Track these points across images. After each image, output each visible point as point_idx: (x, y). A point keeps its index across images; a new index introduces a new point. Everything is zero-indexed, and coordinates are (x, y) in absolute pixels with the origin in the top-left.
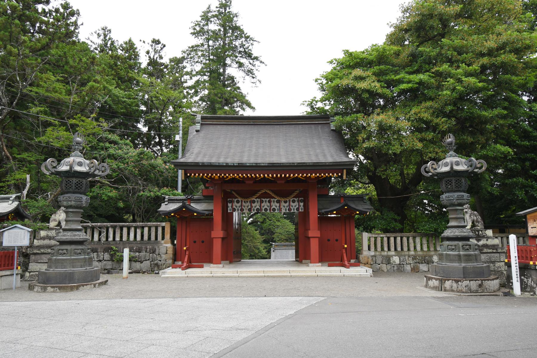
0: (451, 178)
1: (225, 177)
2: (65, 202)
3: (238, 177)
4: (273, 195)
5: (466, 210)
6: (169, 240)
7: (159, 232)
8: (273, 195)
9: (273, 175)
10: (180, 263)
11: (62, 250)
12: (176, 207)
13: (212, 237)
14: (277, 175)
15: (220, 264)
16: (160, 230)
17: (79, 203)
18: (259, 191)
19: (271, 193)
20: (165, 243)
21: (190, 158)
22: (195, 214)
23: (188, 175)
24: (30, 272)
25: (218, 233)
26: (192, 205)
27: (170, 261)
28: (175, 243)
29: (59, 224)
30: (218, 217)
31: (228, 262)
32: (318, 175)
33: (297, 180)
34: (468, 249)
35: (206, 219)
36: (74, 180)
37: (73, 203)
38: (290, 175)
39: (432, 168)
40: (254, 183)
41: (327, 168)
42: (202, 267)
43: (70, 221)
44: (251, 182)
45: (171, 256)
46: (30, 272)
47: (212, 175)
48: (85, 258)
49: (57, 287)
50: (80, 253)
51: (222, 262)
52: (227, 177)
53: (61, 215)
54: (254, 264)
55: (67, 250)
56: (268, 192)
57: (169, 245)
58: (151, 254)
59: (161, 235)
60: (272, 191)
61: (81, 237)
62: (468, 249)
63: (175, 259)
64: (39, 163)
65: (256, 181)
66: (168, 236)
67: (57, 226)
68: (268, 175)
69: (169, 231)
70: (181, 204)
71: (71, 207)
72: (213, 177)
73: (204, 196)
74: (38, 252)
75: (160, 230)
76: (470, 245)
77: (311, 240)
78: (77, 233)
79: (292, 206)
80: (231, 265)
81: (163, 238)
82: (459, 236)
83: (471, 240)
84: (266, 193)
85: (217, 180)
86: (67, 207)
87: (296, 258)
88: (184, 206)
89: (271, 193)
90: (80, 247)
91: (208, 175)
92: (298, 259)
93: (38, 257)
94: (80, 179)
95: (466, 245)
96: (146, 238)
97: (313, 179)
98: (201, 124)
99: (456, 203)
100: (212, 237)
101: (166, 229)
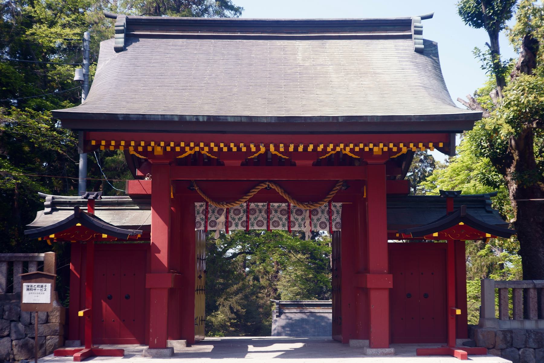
1: (178, 149)
3: (206, 149)
8: (286, 197)
9: (287, 147)
12: (63, 219)
13: (147, 286)
14: (296, 148)
18: (259, 183)
19: (278, 190)
21: (92, 103)
22: (105, 236)
23: (93, 143)
26: (97, 213)
32: (361, 146)
33: (340, 160)
40: (242, 164)
44: (238, 163)
47: (148, 144)
56: (274, 187)
65: (250, 163)
68: (277, 148)
70: (72, 212)
72: (150, 149)
79: (234, 219)
84: (268, 189)
85: (159, 157)
87: (333, 334)
88: (79, 216)
89: (278, 190)
91: (138, 145)
92: (341, 337)
97: (378, 157)
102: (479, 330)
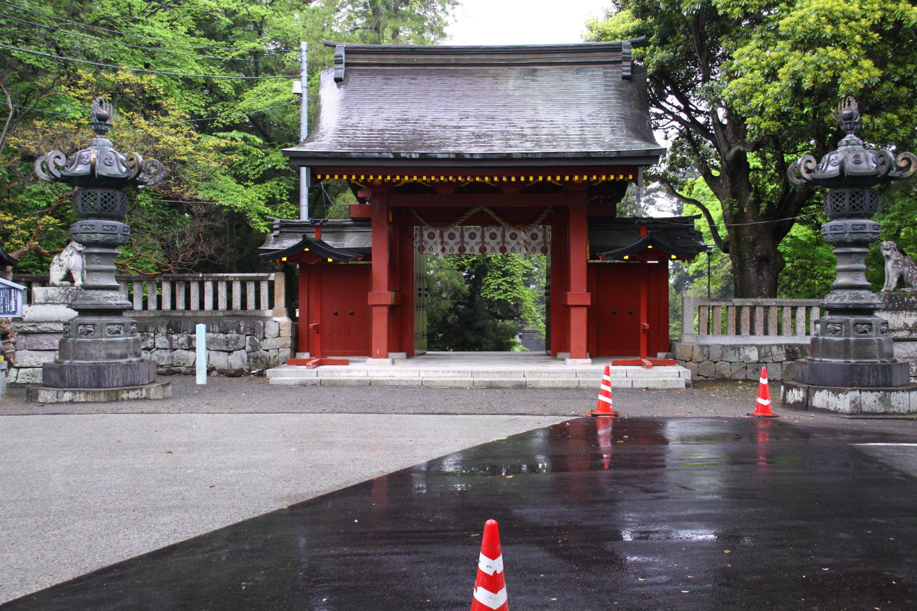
0: (844, 190)
2: (85, 236)
4: (498, 220)
5: (888, 253)
6: (284, 309)
7: (262, 293)
8: (498, 220)
10: (306, 356)
11: (85, 325)
13: (370, 303)
15: (387, 357)
16: (264, 287)
17: (111, 237)
19: (491, 213)
20: (275, 315)
23: (319, 177)
24: (19, 368)
25: (382, 294)
27: (287, 352)
28: (297, 315)
29: (69, 277)
30: (380, 267)
31: (404, 354)
34: (865, 332)
35: (356, 269)
36: (99, 193)
37: (99, 237)
38: (527, 179)
39: (806, 168)
41: (604, 163)
42: (346, 363)
43: (96, 271)
45: (289, 342)
46: (19, 368)
48: (127, 341)
49: (405, 159)
50: (118, 332)
51: (391, 354)
52: (399, 182)
53: (70, 259)
54: (447, 358)
55: (93, 325)
56: (487, 210)
57: (284, 320)
58: (248, 338)
59: (267, 298)
60: (493, 209)
61: (118, 302)
62: (865, 332)
63: (296, 348)
64: (268, 277)
66: (280, 301)
67: (65, 279)
69: (283, 291)
70: (301, 240)
71: (96, 244)
73: (354, 219)
74: (32, 329)
75: (264, 287)
76: (870, 324)
77: (573, 311)
78: (111, 294)
80: (410, 361)
81: (271, 305)
82: (850, 306)
83: (877, 314)
85: (377, 186)
86: (87, 244)
88: (306, 242)
89: (491, 213)
90: (116, 320)
92: (549, 352)
93: (32, 338)
94: (111, 191)
95: (863, 324)
96: (237, 304)
98: (347, 65)
99: (849, 240)
100: (370, 303)
101: (276, 287)
102: (677, 344)
